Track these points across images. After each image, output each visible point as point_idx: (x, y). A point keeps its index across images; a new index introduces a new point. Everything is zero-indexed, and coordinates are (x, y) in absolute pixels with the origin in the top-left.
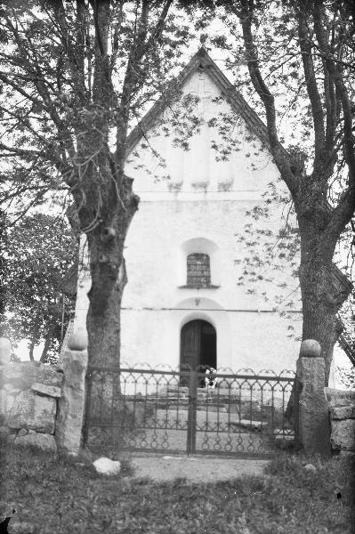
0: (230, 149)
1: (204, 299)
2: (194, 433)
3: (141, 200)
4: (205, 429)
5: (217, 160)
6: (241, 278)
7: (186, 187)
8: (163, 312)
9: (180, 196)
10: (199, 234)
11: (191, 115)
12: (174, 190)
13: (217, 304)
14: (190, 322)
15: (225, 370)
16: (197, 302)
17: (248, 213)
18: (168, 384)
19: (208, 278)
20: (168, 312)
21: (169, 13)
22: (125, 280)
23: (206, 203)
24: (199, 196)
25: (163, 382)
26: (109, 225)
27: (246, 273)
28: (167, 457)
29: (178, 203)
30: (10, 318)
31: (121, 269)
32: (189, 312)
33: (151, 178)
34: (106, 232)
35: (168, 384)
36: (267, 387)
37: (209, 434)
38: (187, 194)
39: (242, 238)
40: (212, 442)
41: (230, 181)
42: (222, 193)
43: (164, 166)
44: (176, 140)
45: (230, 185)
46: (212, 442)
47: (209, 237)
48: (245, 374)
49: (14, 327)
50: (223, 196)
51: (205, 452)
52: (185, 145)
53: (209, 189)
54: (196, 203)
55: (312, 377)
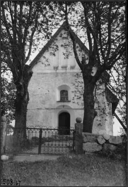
0: (69, 54)
1: (65, 105)
2: (41, 148)
3: (34, 73)
4: (48, 146)
5: (65, 58)
6: (74, 98)
7: (60, 68)
8: (52, 110)
9: (58, 71)
10: (64, 84)
11: (55, 44)
12: (55, 69)
13: (71, 107)
14: (61, 114)
15: (31, 127)
16: (64, 106)
17: (75, 76)
18: (52, 133)
19: (67, 98)
20: (53, 110)
21: (5, 14)
22: (28, 99)
23: (66, 73)
24: (64, 71)
25: (54, 132)
26: (20, 81)
27: (75, 96)
28: (31, 156)
29: (57, 73)
30: (9, 113)
31: (26, 96)
32: (60, 110)
33: (43, 65)
34: (19, 84)
35: (52, 133)
36: (31, 131)
37: (45, 148)
38: (60, 71)
39: (74, 84)
40: (46, 150)
41: (74, 65)
42: (72, 70)
43: (47, 61)
44: (51, 53)
45: (58, 67)
46: (46, 150)
47: (67, 85)
48: (51, 128)
49: (11, 116)
50: (72, 71)
51: (44, 154)
52: (54, 55)
53: (67, 68)
54: (63, 73)
55: (79, 129)
